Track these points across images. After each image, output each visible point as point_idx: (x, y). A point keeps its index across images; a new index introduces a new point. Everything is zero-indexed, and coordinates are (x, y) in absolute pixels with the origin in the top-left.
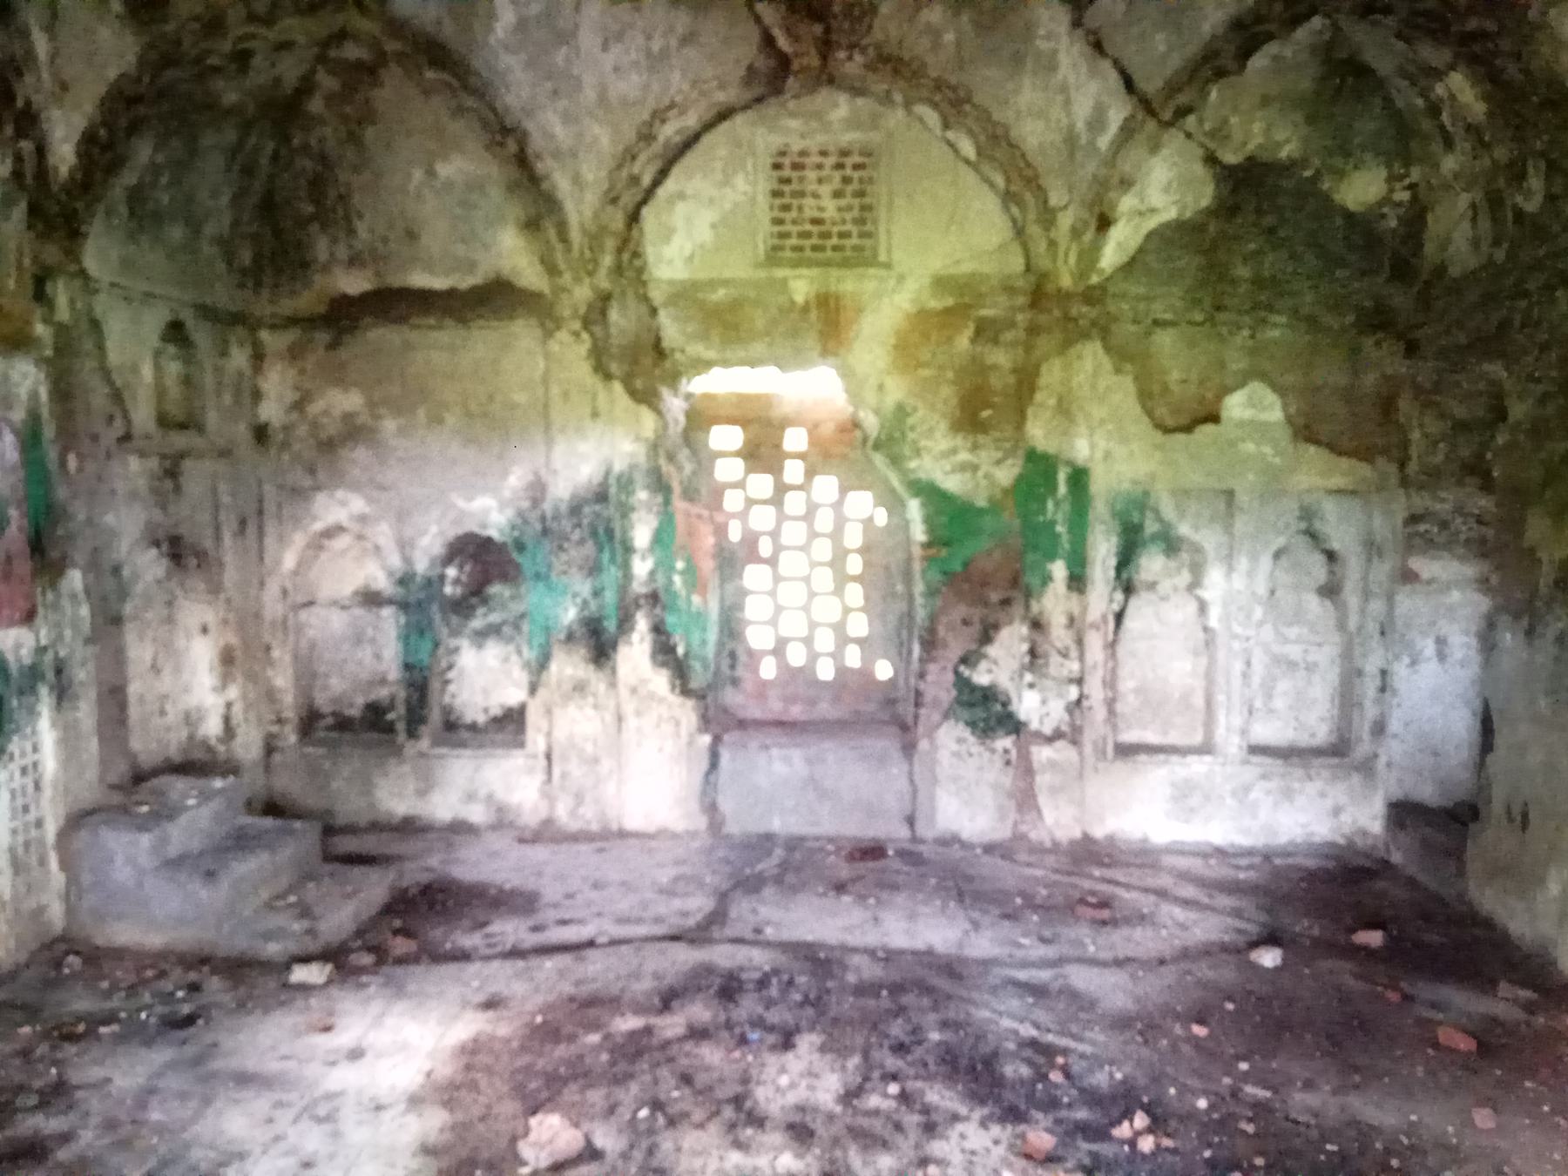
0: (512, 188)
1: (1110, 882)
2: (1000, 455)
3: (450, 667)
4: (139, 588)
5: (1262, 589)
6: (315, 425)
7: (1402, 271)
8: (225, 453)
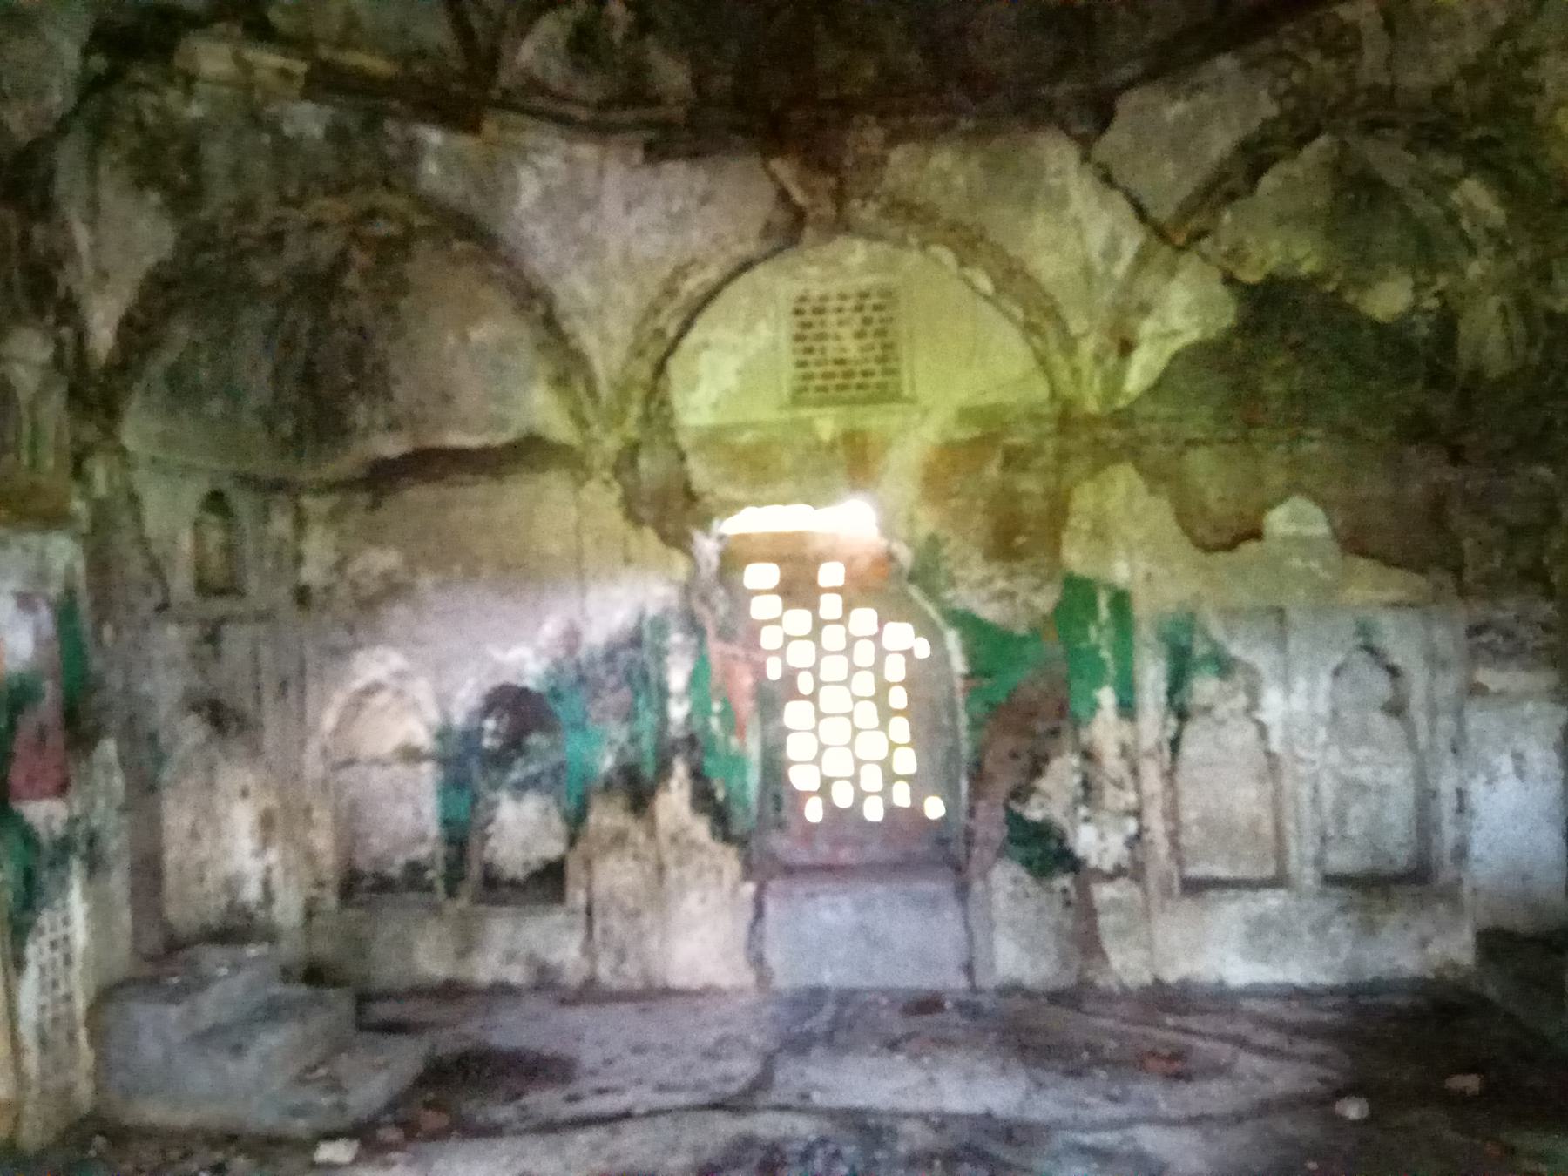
0: (541, 347)
1: (1186, 1031)
2: (1037, 581)
3: (490, 821)
4: (179, 753)
5: (1323, 707)
6: (355, 585)
7: (1437, 379)
8: (263, 617)
